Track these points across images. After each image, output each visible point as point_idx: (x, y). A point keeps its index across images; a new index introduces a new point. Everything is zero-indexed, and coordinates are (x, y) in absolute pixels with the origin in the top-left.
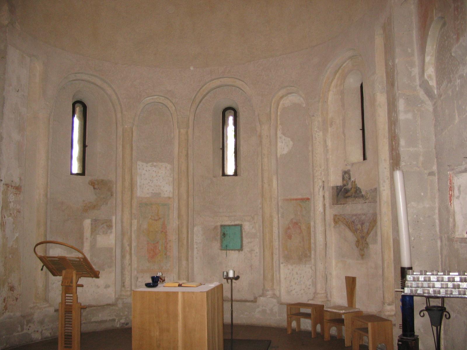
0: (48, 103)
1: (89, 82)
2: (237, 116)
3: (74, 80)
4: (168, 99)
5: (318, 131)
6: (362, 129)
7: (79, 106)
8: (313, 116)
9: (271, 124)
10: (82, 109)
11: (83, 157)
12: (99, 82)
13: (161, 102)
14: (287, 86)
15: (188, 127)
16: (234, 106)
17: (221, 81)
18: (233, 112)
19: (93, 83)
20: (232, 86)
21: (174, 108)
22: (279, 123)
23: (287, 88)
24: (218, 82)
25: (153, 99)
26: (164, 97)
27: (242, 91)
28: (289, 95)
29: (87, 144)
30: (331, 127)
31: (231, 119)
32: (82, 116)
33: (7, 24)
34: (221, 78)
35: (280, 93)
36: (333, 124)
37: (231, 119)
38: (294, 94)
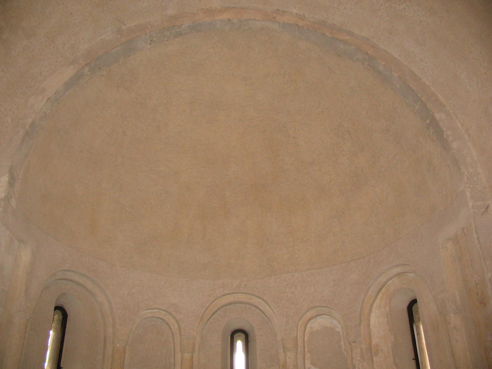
0: (29, 304)
1: (78, 284)
2: (249, 340)
3: (61, 279)
4: (170, 314)
5: (361, 360)
6: (414, 358)
7: (58, 314)
8: (354, 342)
9: (297, 350)
10: (61, 317)
11: (410, 326)
12: (89, 285)
13: (161, 317)
14: (317, 307)
15: (193, 352)
16: (246, 328)
17: (234, 297)
18: (243, 336)
19: (82, 285)
20: (246, 304)
21: (176, 326)
22: (306, 350)
23: (317, 309)
24: (230, 299)
25: (151, 312)
26: (165, 311)
27: (259, 311)
28: (318, 317)
29: (62, 365)
30: (376, 356)
31: (239, 345)
32: (59, 327)
33: (3, 197)
34: (234, 293)
35: (308, 315)
36: (379, 352)
37: (239, 345)
38: (324, 316)
